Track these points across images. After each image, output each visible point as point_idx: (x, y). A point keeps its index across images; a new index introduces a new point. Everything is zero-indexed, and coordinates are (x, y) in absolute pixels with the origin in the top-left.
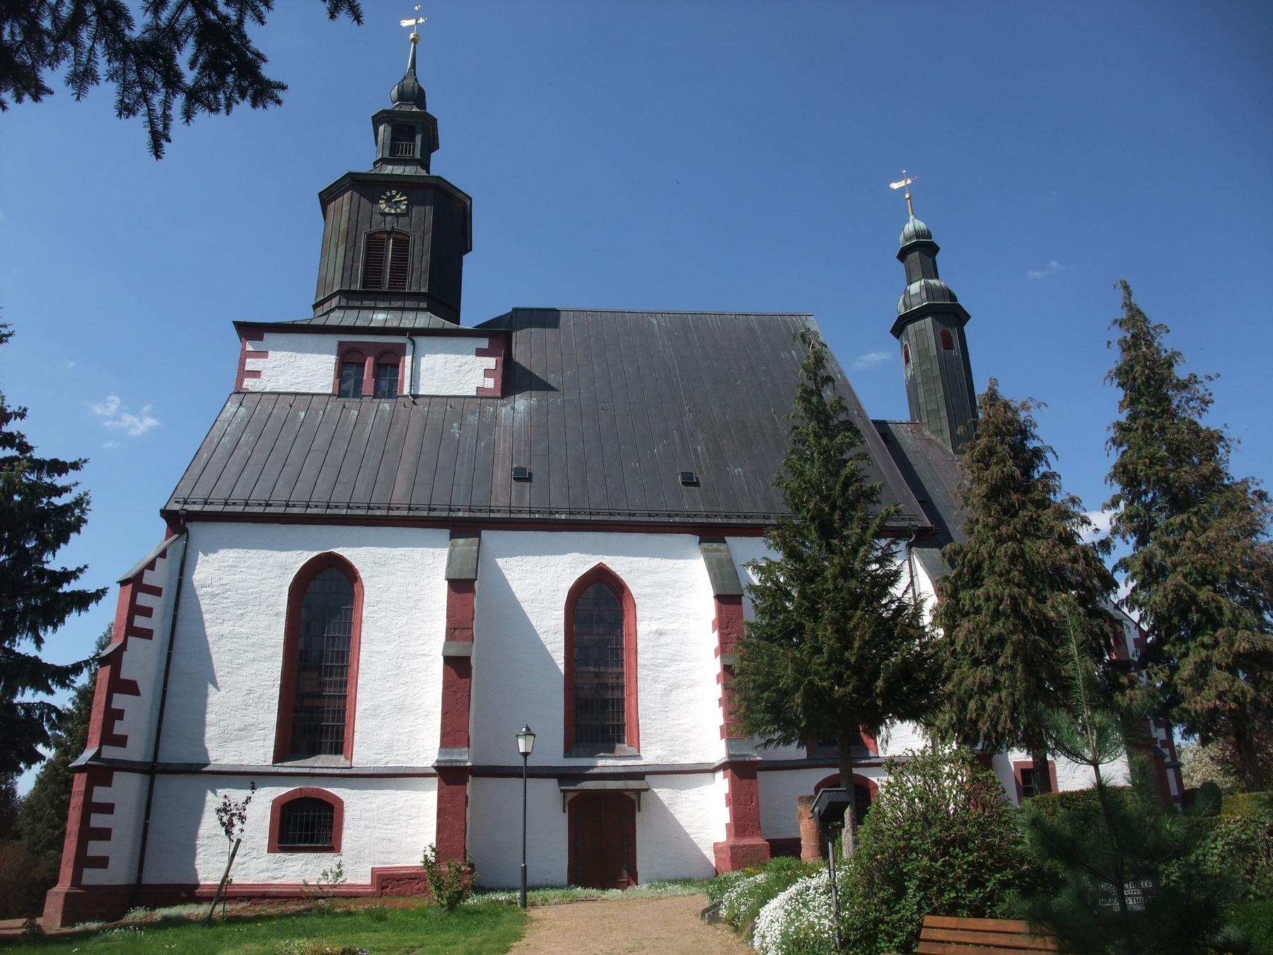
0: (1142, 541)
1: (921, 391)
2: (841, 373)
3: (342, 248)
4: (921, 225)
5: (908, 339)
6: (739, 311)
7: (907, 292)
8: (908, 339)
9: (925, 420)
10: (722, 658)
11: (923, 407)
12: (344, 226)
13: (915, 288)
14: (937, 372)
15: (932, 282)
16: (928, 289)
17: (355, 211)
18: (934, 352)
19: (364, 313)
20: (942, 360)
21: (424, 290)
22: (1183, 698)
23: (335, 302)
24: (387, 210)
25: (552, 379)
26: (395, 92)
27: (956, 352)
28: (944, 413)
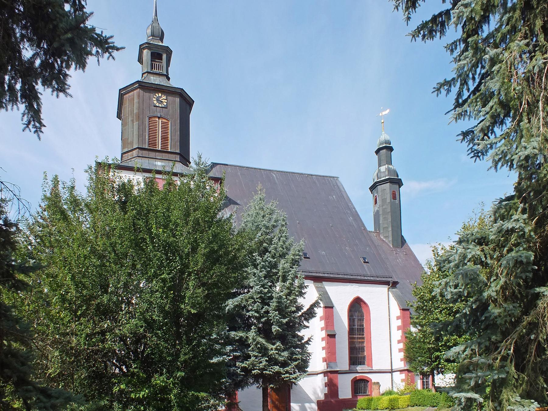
0: (298, 287)
1: (381, 218)
2: (355, 208)
3: (136, 124)
4: (388, 138)
5: (377, 193)
6: (309, 173)
7: (379, 171)
8: (377, 193)
9: (382, 231)
10: (326, 331)
11: (381, 225)
12: (135, 111)
13: (383, 169)
14: (389, 210)
15: (390, 166)
16: (389, 170)
17: (142, 102)
18: (388, 201)
19: (151, 161)
20: (392, 204)
21: (178, 151)
22: (486, 346)
23: (135, 153)
24: (157, 105)
25: (238, 202)
26: (149, 31)
27: (397, 201)
28: (390, 229)
